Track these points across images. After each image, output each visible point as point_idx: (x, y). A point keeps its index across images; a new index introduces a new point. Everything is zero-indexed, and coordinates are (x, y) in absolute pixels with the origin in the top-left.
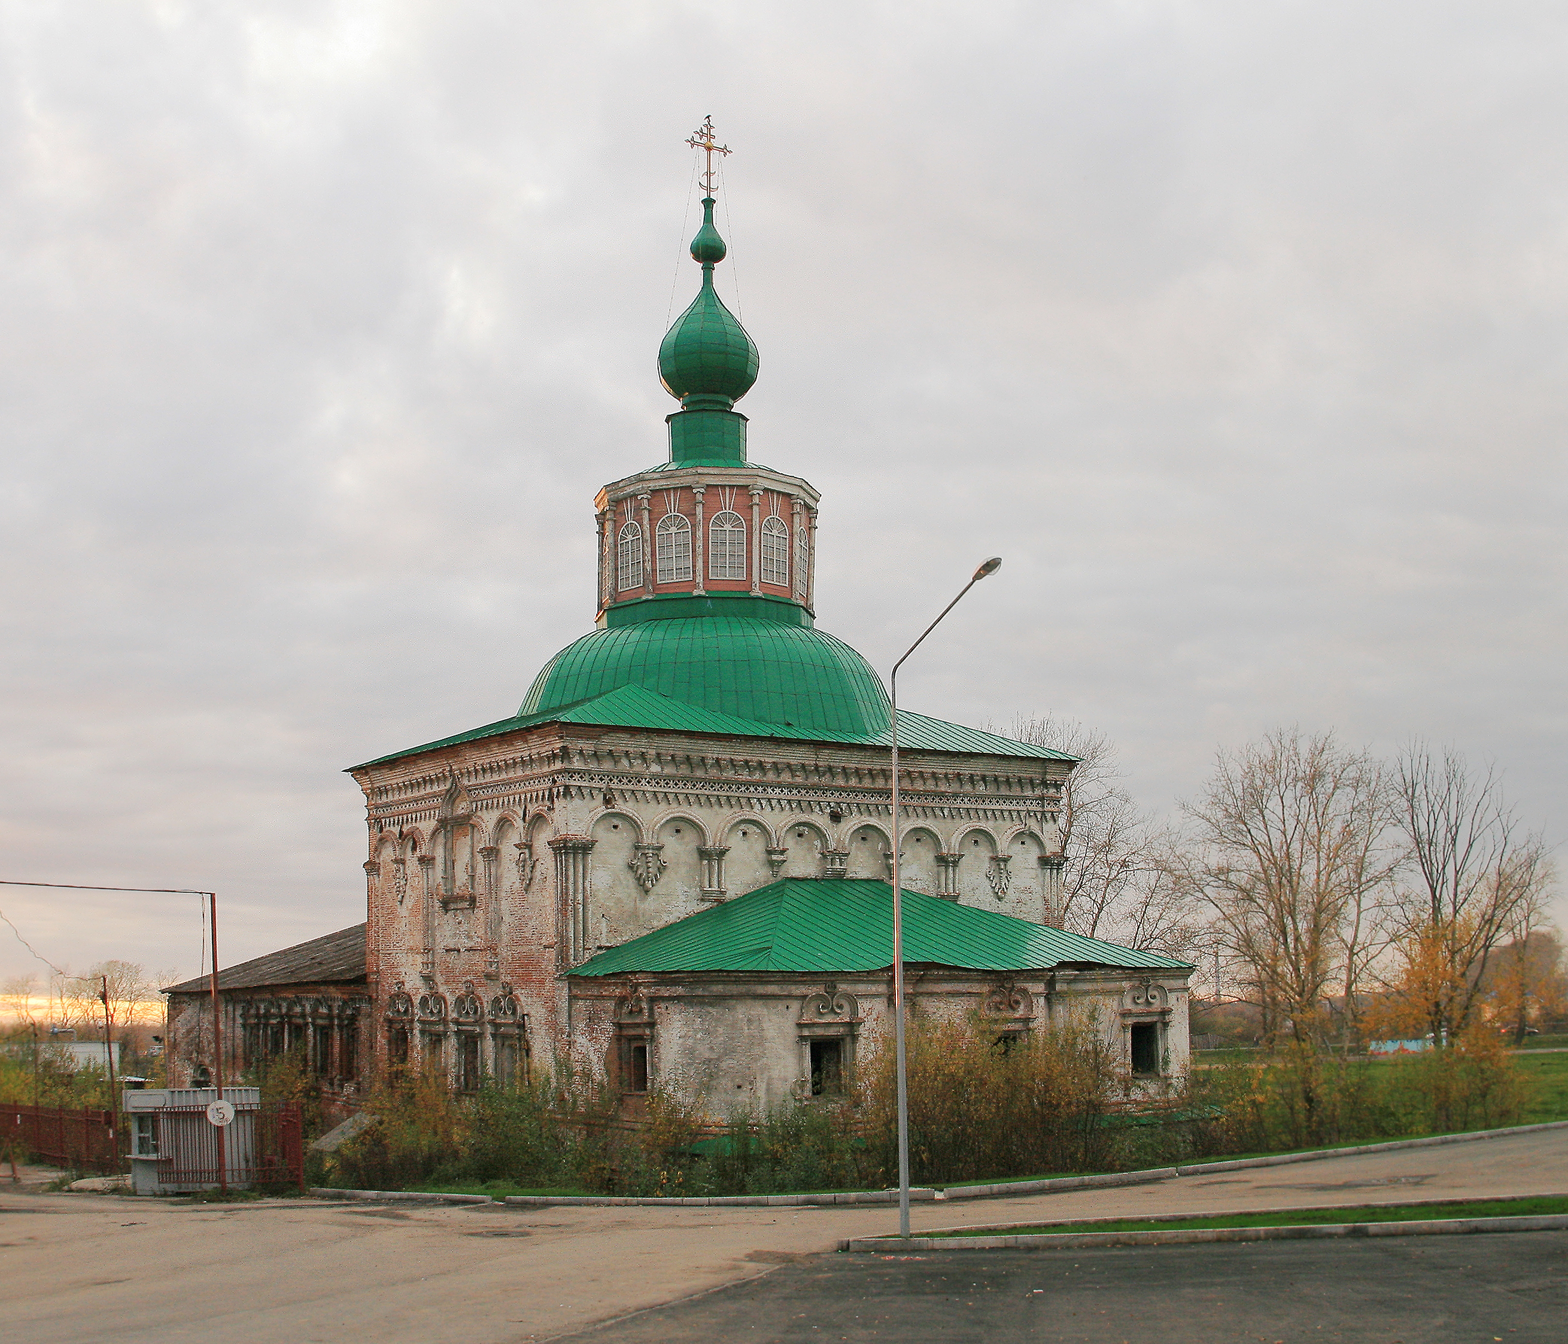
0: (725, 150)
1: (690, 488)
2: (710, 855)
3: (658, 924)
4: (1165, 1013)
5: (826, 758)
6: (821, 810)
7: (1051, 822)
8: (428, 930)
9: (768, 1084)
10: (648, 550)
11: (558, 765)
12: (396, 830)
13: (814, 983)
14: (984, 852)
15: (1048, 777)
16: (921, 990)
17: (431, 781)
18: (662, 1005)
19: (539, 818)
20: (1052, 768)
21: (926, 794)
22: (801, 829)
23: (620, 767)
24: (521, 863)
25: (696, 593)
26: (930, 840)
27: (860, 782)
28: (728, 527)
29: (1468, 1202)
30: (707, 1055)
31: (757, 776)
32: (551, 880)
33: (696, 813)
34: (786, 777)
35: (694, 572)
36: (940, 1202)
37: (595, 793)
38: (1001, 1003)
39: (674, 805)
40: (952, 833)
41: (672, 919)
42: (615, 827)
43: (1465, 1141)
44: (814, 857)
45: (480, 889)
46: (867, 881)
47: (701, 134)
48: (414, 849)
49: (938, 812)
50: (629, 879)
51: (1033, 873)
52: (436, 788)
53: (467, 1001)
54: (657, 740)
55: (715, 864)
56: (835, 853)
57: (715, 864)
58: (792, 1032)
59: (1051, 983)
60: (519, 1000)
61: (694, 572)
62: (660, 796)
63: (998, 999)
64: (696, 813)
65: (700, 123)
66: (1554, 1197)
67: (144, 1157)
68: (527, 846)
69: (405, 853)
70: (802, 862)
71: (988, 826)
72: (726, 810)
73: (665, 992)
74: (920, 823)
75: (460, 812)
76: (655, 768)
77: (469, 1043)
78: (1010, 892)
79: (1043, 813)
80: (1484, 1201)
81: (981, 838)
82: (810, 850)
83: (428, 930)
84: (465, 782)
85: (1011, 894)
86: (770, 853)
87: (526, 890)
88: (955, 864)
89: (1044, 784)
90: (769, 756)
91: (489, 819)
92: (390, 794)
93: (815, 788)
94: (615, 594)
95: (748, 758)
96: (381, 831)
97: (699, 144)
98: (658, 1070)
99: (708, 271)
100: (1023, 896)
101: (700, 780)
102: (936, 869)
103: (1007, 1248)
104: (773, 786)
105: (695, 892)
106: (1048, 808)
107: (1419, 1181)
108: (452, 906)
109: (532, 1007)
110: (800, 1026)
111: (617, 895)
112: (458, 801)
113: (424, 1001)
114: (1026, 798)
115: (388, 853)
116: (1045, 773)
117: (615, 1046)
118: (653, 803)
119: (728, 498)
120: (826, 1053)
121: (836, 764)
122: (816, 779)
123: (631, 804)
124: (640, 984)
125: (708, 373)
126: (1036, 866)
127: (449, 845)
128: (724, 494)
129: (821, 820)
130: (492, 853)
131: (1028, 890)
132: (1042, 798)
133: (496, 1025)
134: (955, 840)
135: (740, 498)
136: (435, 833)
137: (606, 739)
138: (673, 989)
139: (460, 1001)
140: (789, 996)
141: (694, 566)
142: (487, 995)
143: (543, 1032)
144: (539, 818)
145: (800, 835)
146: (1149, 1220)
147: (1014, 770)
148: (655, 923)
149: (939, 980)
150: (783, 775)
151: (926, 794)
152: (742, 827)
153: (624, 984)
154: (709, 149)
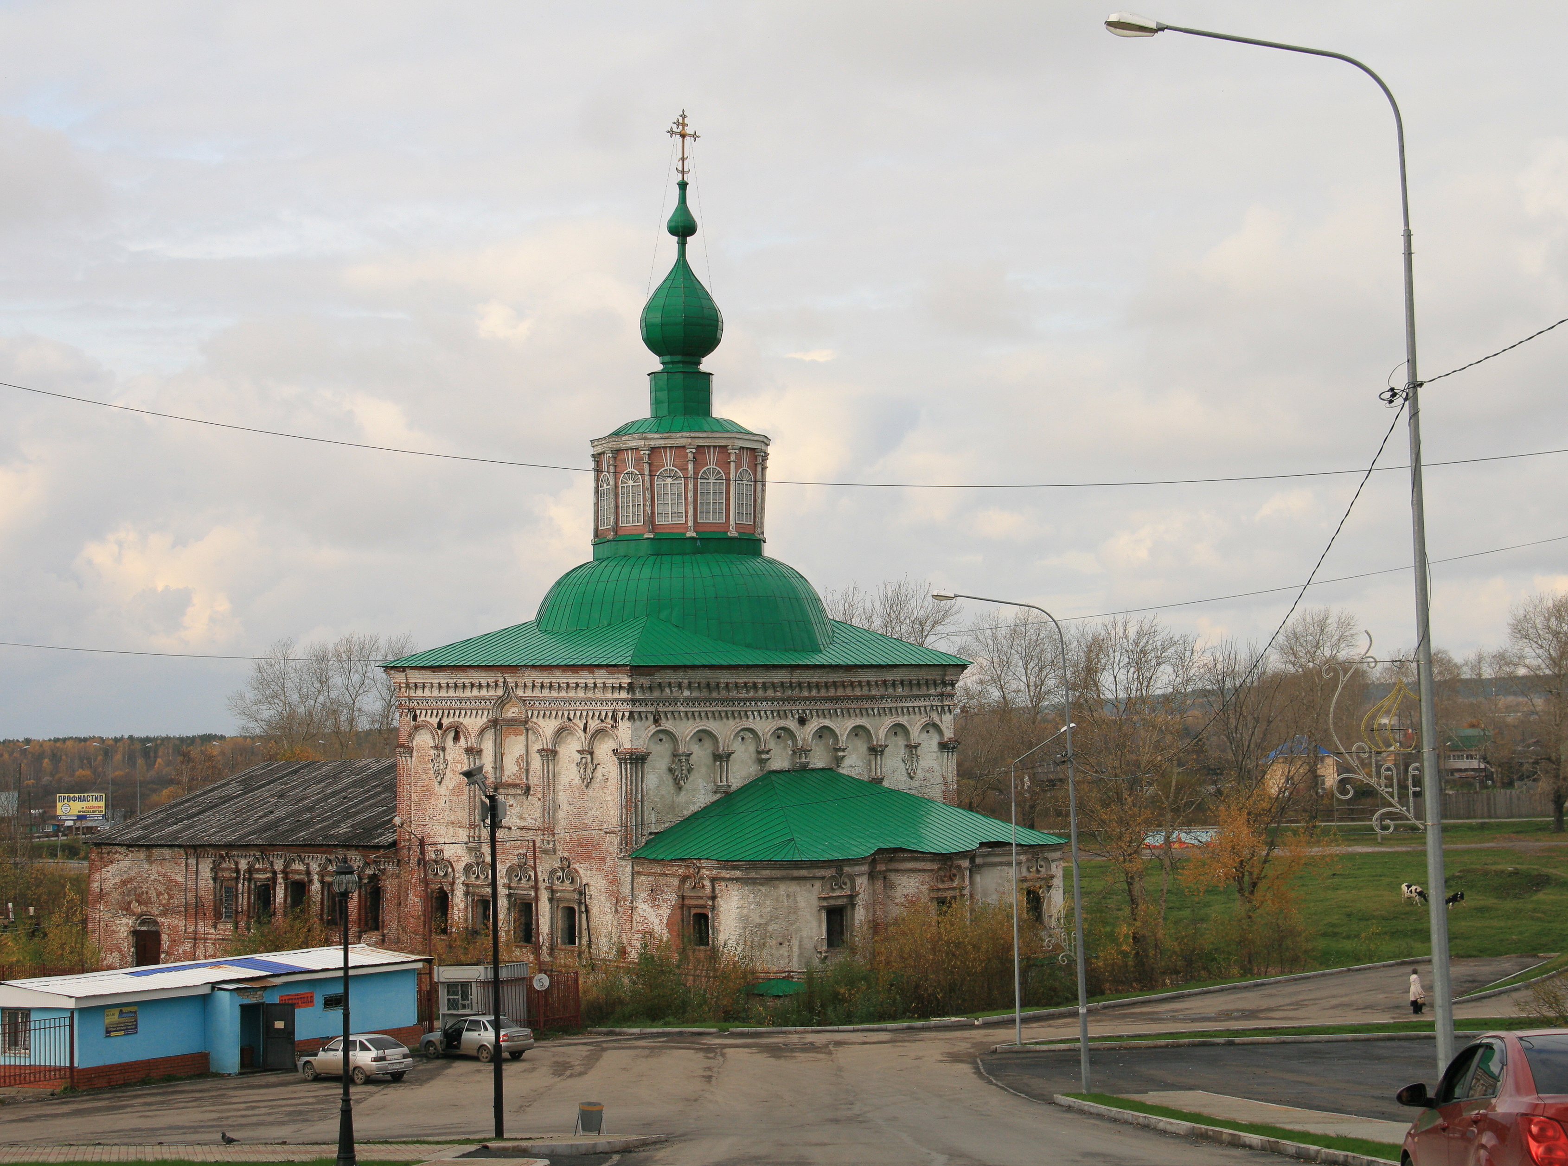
0: (695, 136)
2: (721, 758)
3: (687, 813)
5: (798, 676)
6: (793, 716)
7: (948, 714)
9: (800, 942)
10: (648, 496)
11: (624, 695)
12: (435, 721)
13: (830, 867)
14: (901, 741)
15: (947, 678)
16: (890, 867)
17: (480, 686)
18: (723, 884)
20: (950, 671)
21: (862, 698)
23: (664, 694)
25: (689, 534)
26: (864, 734)
27: (818, 693)
29: (1278, 1028)
30: (758, 920)
33: (712, 726)
35: (686, 516)
36: (978, 1027)
37: (649, 715)
38: (945, 876)
39: (698, 720)
41: (694, 808)
42: (661, 740)
43: (1271, 984)
44: (787, 753)
45: (534, 781)
46: (822, 769)
47: (678, 124)
48: (456, 738)
49: (870, 712)
50: (669, 780)
54: (690, 673)
55: (724, 764)
57: (724, 764)
58: (815, 903)
59: (972, 860)
60: (577, 872)
61: (686, 516)
62: (690, 715)
63: (943, 874)
64: (712, 726)
65: (676, 116)
66: (1322, 1026)
69: (444, 742)
70: (780, 761)
71: (903, 720)
72: (731, 722)
74: (859, 722)
75: (510, 715)
76: (687, 693)
78: (919, 771)
79: (943, 707)
80: (1286, 1028)
81: (899, 730)
82: (785, 748)
84: (520, 693)
85: (920, 774)
86: (759, 753)
87: (587, 787)
88: (882, 752)
89: (944, 684)
90: (760, 678)
91: (548, 727)
92: (426, 690)
93: (788, 699)
96: (415, 718)
97: (676, 133)
98: (718, 931)
99: (682, 244)
100: (928, 775)
101: (715, 700)
102: (868, 757)
103: (1070, 1050)
104: (761, 700)
105: (711, 786)
106: (946, 703)
107: (1252, 1014)
109: (595, 882)
111: (663, 793)
112: (507, 706)
113: (468, 868)
114: (930, 695)
116: (945, 675)
117: (679, 912)
118: (685, 719)
119: (712, 458)
120: (836, 917)
121: (804, 680)
122: (790, 692)
123: (670, 722)
124: (704, 868)
125: (684, 332)
126: (936, 750)
127: (498, 741)
128: (709, 453)
129: (791, 724)
130: (550, 754)
131: (931, 770)
132: (942, 695)
135: (721, 455)
136: (482, 731)
137: (657, 675)
138: (733, 872)
140: (814, 878)
141: (686, 512)
143: (603, 899)
145: (779, 737)
146: (1123, 1036)
147: (923, 675)
148: (685, 812)
149: (905, 860)
150: (768, 692)
151: (862, 698)
152: (742, 734)
153: (687, 867)
154: (683, 136)
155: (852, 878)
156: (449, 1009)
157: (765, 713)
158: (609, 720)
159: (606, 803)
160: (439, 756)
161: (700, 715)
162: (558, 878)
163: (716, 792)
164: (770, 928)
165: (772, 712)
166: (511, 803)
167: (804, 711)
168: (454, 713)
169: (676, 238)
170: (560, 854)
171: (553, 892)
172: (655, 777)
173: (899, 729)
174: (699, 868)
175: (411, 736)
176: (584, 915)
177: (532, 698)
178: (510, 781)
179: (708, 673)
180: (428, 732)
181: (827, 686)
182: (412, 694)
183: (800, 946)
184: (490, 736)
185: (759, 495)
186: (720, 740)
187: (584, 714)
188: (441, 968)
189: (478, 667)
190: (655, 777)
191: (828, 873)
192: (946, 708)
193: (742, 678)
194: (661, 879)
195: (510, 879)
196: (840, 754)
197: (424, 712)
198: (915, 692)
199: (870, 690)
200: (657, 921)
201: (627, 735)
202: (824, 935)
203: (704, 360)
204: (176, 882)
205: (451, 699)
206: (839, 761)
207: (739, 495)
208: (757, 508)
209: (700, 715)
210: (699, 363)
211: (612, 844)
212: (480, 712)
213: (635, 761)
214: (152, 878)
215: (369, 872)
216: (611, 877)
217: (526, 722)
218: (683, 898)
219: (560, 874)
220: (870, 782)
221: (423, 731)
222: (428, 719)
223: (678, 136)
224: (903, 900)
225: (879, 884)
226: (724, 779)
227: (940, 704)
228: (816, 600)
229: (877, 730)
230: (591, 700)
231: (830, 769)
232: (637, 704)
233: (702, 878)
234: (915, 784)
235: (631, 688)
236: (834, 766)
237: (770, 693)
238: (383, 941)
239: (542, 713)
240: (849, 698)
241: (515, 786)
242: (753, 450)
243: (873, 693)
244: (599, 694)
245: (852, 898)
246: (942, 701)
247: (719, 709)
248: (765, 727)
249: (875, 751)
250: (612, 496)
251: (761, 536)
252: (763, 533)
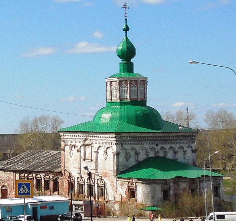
1: (127, 80)
2: (137, 154)
4: (220, 184)
6: (155, 144)
12: (70, 144)
14: (182, 150)
18: (138, 184)
20: (194, 133)
28: (134, 88)
33: (135, 146)
34: (149, 139)
42: (123, 150)
45: (93, 158)
46: (162, 157)
48: (75, 148)
49: (174, 143)
50: (125, 159)
51: (190, 154)
52: (81, 137)
58: (160, 189)
70: (152, 155)
71: (182, 145)
72: (139, 145)
74: (171, 145)
79: (192, 142)
85: (187, 158)
86: (147, 152)
88: (177, 153)
89: (193, 136)
91: (96, 146)
95: (143, 136)
97: (124, 8)
99: (126, 33)
105: (135, 161)
108: (86, 160)
110: (162, 188)
125: (128, 54)
130: (97, 152)
134: (177, 148)
140: (160, 183)
156: (76, 210)
157: (148, 143)
158: (110, 145)
160: (71, 152)
161: (134, 144)
162: (99, 181)
163: (136, 162)
165: (149, 143)
166: (88, 163)
167: (157, 143)
168: (77, 142)
169: (124, 32)
170: (100, 175)
171: (98, 184)
174: (132, 180)
175: (64, 147)
176: (105, 190)
177: (92, 139)
178: (87, 158)
179: (134, 134)
180: (68, 146)
181: (163, 136)
182: (64, 137)
184: (83, 147)
185: (145, 91)
186: (137, 150)
187: (105, 143)
188: (74, 201)
189: (80, 132)
192: (193, 142)
193: (142, 135)
194: (123, 182)
196: (167, 153)
197: (67, 141)
198: (185, 138)
199: (174, 138)
200: (123, 192)
202: (163, 196)
203: (132, 59)
204: (11, 178)
205: (73, 139)
206: (166, 155)
207: (141, 91)
208: (145, 95)
209: (134, 144)
210: (131, 60)
211: (112, 173)
212: (80, 142)
214: (5, 177)
215: (55, 178)
216: (111, 181)
217: (91, 145)
218: (129, 187)
219: (99, 180)
220: (174, 160)
221: (67, 146)
222: (68, 143)
223: (125, 8)
224: (182, 189)
226: (138, 159)
227: (192, 141)
228: (160, 116)
229: (176, 147)
231: (164, 157)
232: (117, 141)
233: (133, 182)
234: (186, 160)
236: (165, 156)
237: (149, 139)
238: (59, 194)
239: (95, 143)
241: (89, 159)
243: (175, 138)
245: (170, 187)
246: (192, 140)
247: (134, 142)
248: (147, 146)
249: (175, 152)
250: (110, 92)
251: (146, 101)
252: (146, 100)
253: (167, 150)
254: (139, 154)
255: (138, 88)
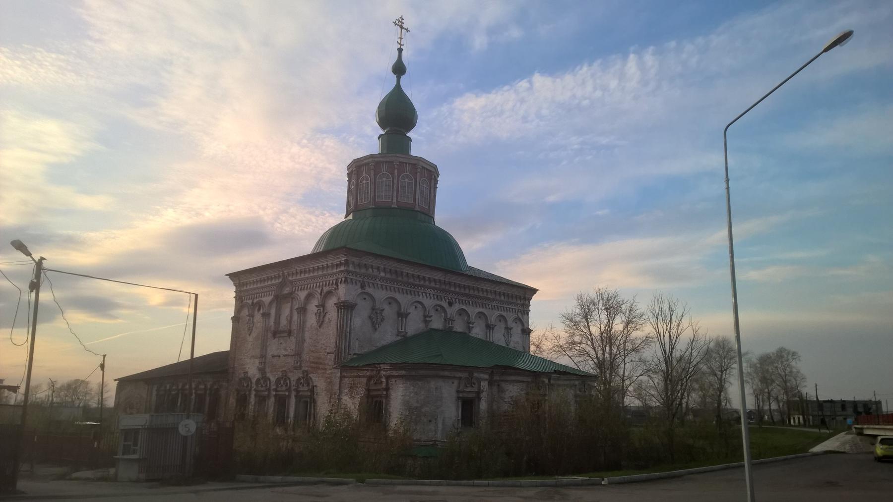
2: (402, 316)
3: (379, 345)
8: (264, 347)
11: (342, 268)
12: (250, 302)
18: (394, 380)
19: (329, 293)
22: (439, 308)
24: (318, 314)
30: (415, 405)
31: (422, 283)
32: (334, 322)
33: (398, 296)
40: (493, 316)
41: (384, 343)
46: (461, 333)
52: (273, 282)
53: (283, 379)
56: (450, 319)
58: (454, 394)
64: (398, 296)
67: (125, 457)
68: (322, 305)
70: (437, 323)
71: (504, 314)
72: (409, 297)
73: (395, 373)
74: (481, 310)
75: (285, 292)
76: (382, 274)
77: (282, 402)
83: (264, 347)
84: (290, 278)
86: (425, 316)
88: (493, 329)
90: (428, 274)
91: (302, 295)
93: (444, 291)
94: (356, 205)
109: (320, 383)
110: (458, 392)
113: (258, 380)
115: (245, 312)
120: (468, 406)
125: (397, 116)
129: (445, 304)
130: (303, 310)
131: (517, 343)
133: (298, 391)
136: (271, 303)
139: (278, 381)
140: (454, 377)
142: (293, 377)
144: (329, 293)
153: (372, 370)
155: (479, 380)
159: (329, 337)
163: (398, 335)
164: (423, 410)
172: (359, 320)
173: (502, 318)
183: (443, 423)
190: (359, 320)
191: (464, 375)
195: (277, 386)
198: (510, 300)
201: (343, 292)
202: (460, 417)
206: (470, 329)
213: (346, 307)
224: (510, 400)
225: (495, 388)
230: (325, 275)
233: (381, 377)
235: (346, 263)
240: (476, 297)
242: (430, 171)
244: (330, 271)
245: (479, 393)
248: (429, 302)
249: (489, 327)
253: (472, 319)
254: (407, 315)
255: (416, 182)
